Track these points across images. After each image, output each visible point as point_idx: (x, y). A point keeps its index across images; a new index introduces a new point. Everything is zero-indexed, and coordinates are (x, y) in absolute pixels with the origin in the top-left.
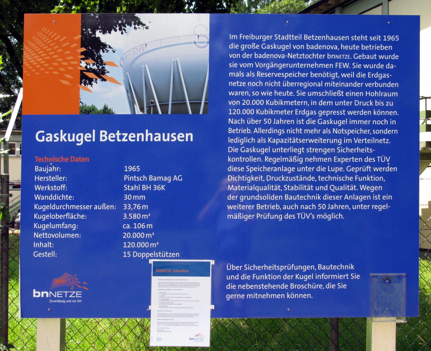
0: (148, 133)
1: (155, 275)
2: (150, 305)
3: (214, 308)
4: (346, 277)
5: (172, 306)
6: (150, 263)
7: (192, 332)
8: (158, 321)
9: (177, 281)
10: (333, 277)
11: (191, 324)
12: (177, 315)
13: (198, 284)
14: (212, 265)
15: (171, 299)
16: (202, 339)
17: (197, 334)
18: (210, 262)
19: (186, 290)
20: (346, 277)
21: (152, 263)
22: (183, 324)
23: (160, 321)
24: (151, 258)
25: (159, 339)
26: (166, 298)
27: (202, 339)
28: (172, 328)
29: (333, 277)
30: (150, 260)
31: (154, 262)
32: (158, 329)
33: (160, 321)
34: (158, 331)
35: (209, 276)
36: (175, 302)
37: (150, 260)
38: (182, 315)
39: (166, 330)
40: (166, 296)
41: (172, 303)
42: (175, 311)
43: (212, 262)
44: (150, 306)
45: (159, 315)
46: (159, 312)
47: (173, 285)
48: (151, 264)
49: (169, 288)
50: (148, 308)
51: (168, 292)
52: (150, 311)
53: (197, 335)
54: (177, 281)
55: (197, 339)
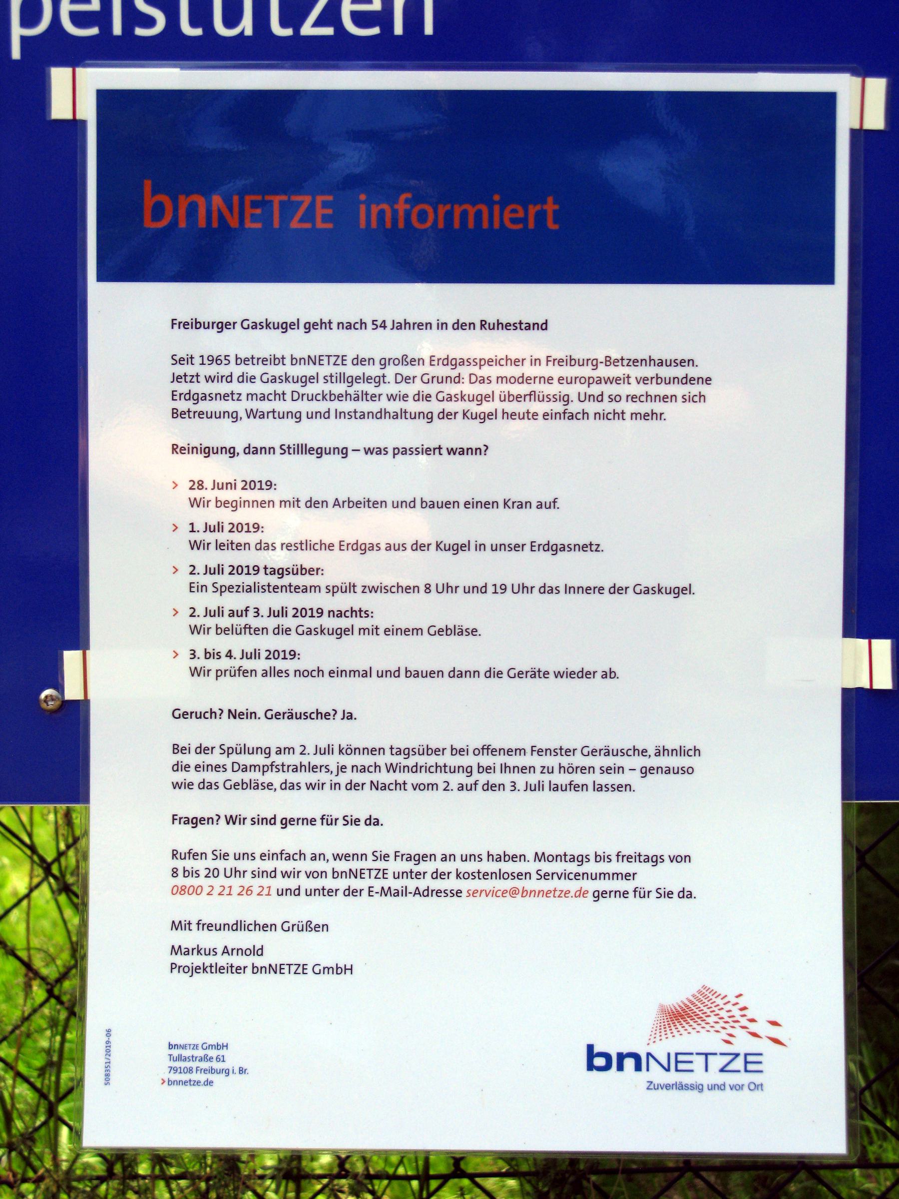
0: (154, 192)
1: (129, 263)
2: (78, 639)
3: (884, 681)
4: (541, 216)
5: (356, 651)
6: (60, 109)
7: (609, 970)
8: (187, 838)
9: (426, 345)
10: (464, 214)
11: (604, 876)
12: (412, 766)
13: (684, 378)
14: (859, 136)
15: (338, 568)
16: (751, 1062)
17: (675, 997)
18: (828, 100)
19: (525, 454)
20: (541, 216)
21: (88, 112)
22: (502, 872)
23: (202, 839)
24: (77, 54)
25: (195, 1064)
26: (280, 558)
27: (751, 1062)
28: (355, 925)
29: (464, 214)
30: (60, 77)
31: (105, 98)
32: (187, 939)
33: (202, 839)
34: (189, 963)
35: (829, 279)
36: (388, 610)
37: (60, 77)
38: (485, 769)
39: (279, 947)
40: (283, 525)
41: (351, 622)
42: (389, 716)
43: (858, 101)
44: (71, 658)
45: (192, 767)
46: (193, 733)
47: (354, 388)
48: (73, 128)
49: (314, 433)
50: (56, 681)
51: (294, 476)
52: (76, 714)
53: (678, 1016)
54: (426, 345)
55: (676, 1062)
